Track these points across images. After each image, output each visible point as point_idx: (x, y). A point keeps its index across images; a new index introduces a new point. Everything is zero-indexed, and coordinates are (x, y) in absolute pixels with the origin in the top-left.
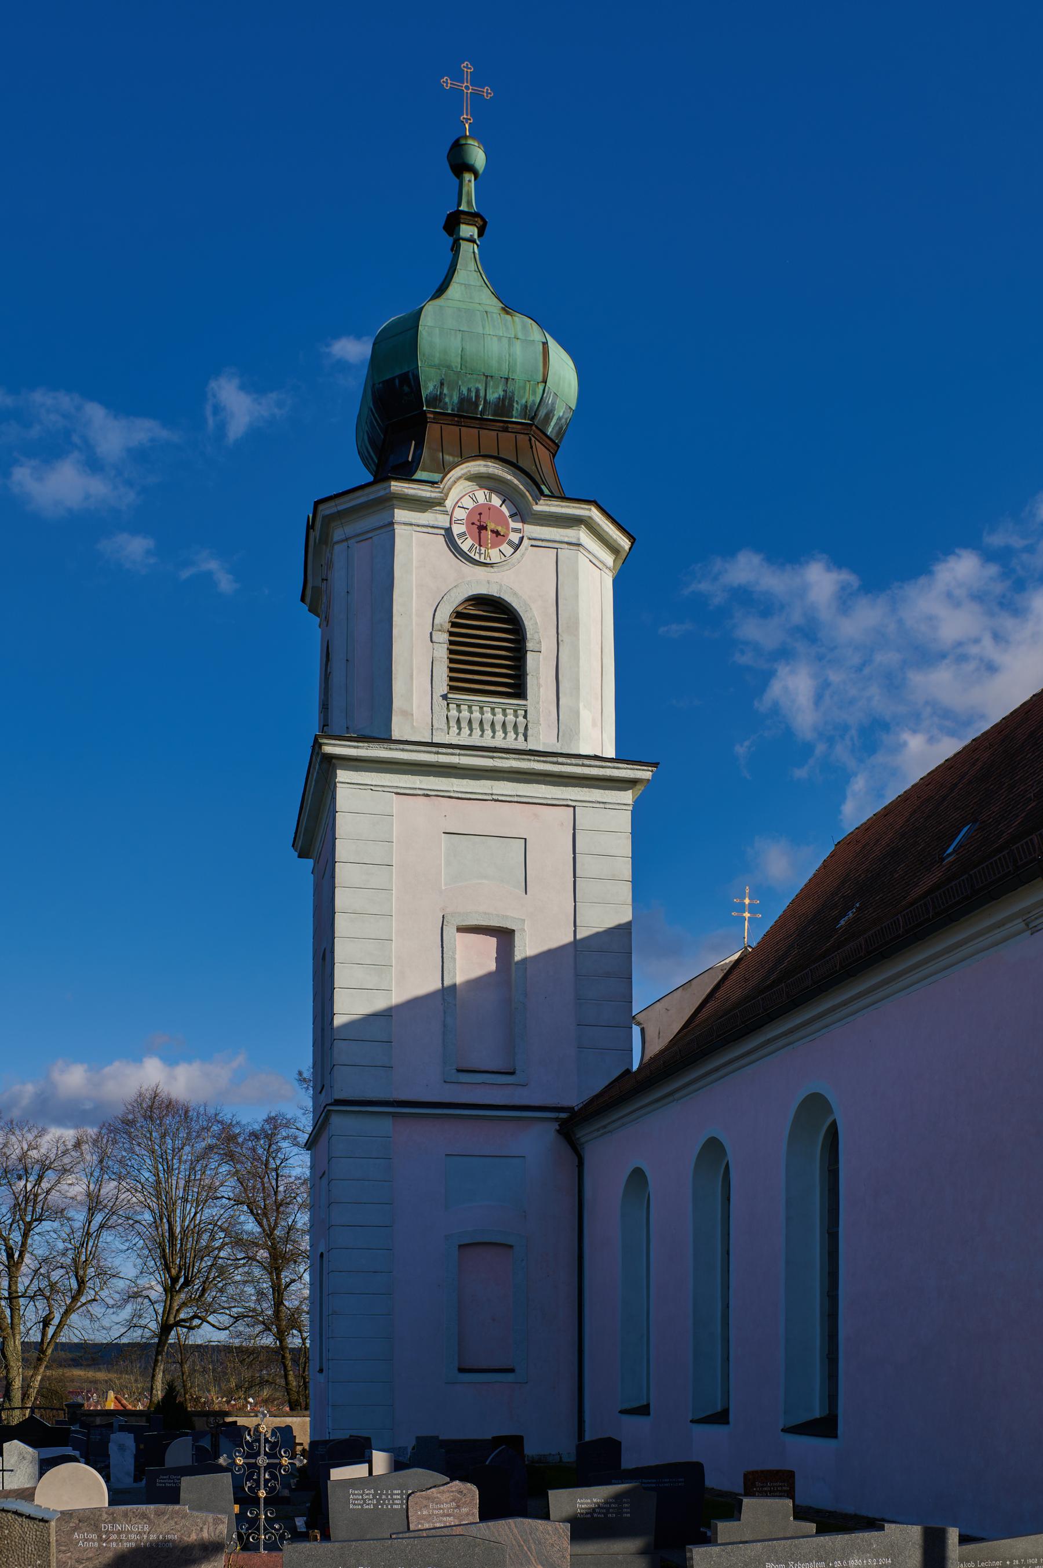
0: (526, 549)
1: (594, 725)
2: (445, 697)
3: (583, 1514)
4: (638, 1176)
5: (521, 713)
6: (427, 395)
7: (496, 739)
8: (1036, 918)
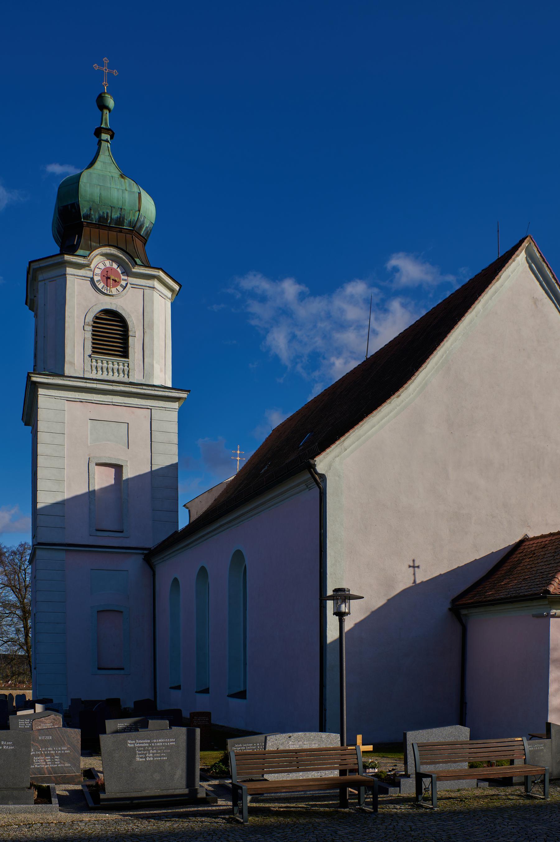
0: (129, 289)
1: (161, 371)
2: (90, 356)
3: (120, 730)
4: (176, 580)
5: (126, 365)
6: (83, 214)
7: (114, 376)
8: (310, 484)
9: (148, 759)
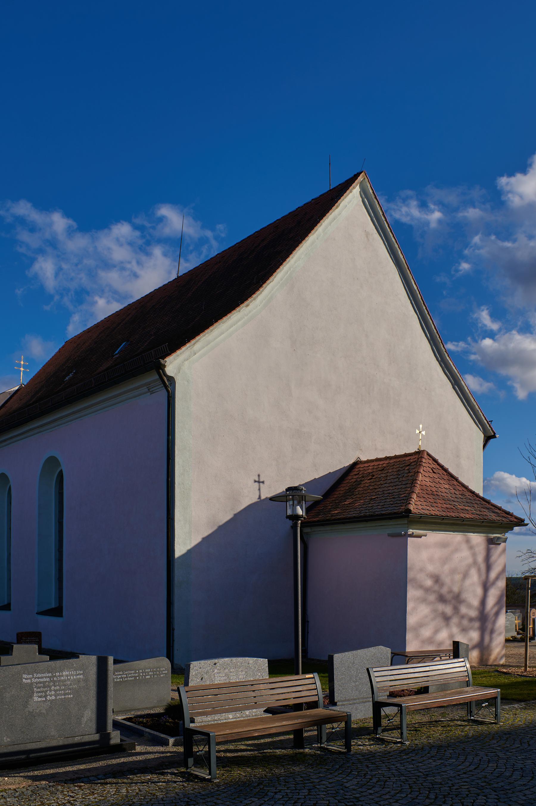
8: (153, 388)
9: (48, 698)
